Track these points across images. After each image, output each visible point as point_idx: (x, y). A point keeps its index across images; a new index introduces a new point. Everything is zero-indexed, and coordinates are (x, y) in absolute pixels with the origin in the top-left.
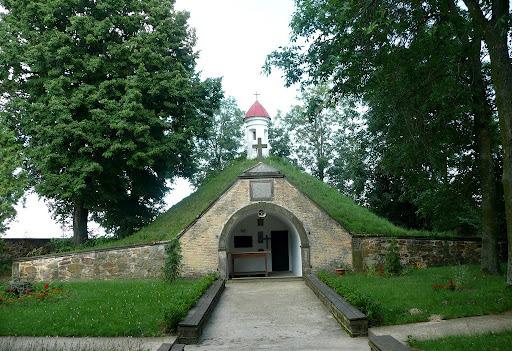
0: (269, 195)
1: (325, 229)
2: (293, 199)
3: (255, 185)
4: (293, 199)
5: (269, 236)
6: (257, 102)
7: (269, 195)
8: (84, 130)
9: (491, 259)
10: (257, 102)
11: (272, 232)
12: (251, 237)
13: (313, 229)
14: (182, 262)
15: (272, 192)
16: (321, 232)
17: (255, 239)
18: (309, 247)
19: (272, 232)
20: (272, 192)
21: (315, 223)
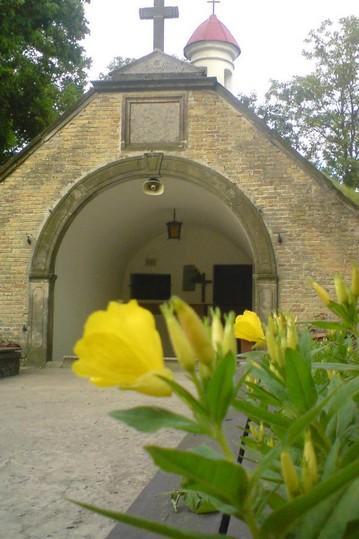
0: (173, 134)
1: (324, 229)
2: (240, 147)
3: (137, 110)
4: (240, 147)
5: (210, 276)
6: (213, 17)
7: (173, 134)
8: (34, 498)
9: (209, 96)
10: (213, 17)
11: (218, 269)
12: (167, 278)
13: (291, 229)
14: (83, 54)
15: (183, 127)
16: (314, 239)
17: (177, 281)
18: (277, 280)
19: (218, 269)
20: (183, 127)
21: (298, 211)
